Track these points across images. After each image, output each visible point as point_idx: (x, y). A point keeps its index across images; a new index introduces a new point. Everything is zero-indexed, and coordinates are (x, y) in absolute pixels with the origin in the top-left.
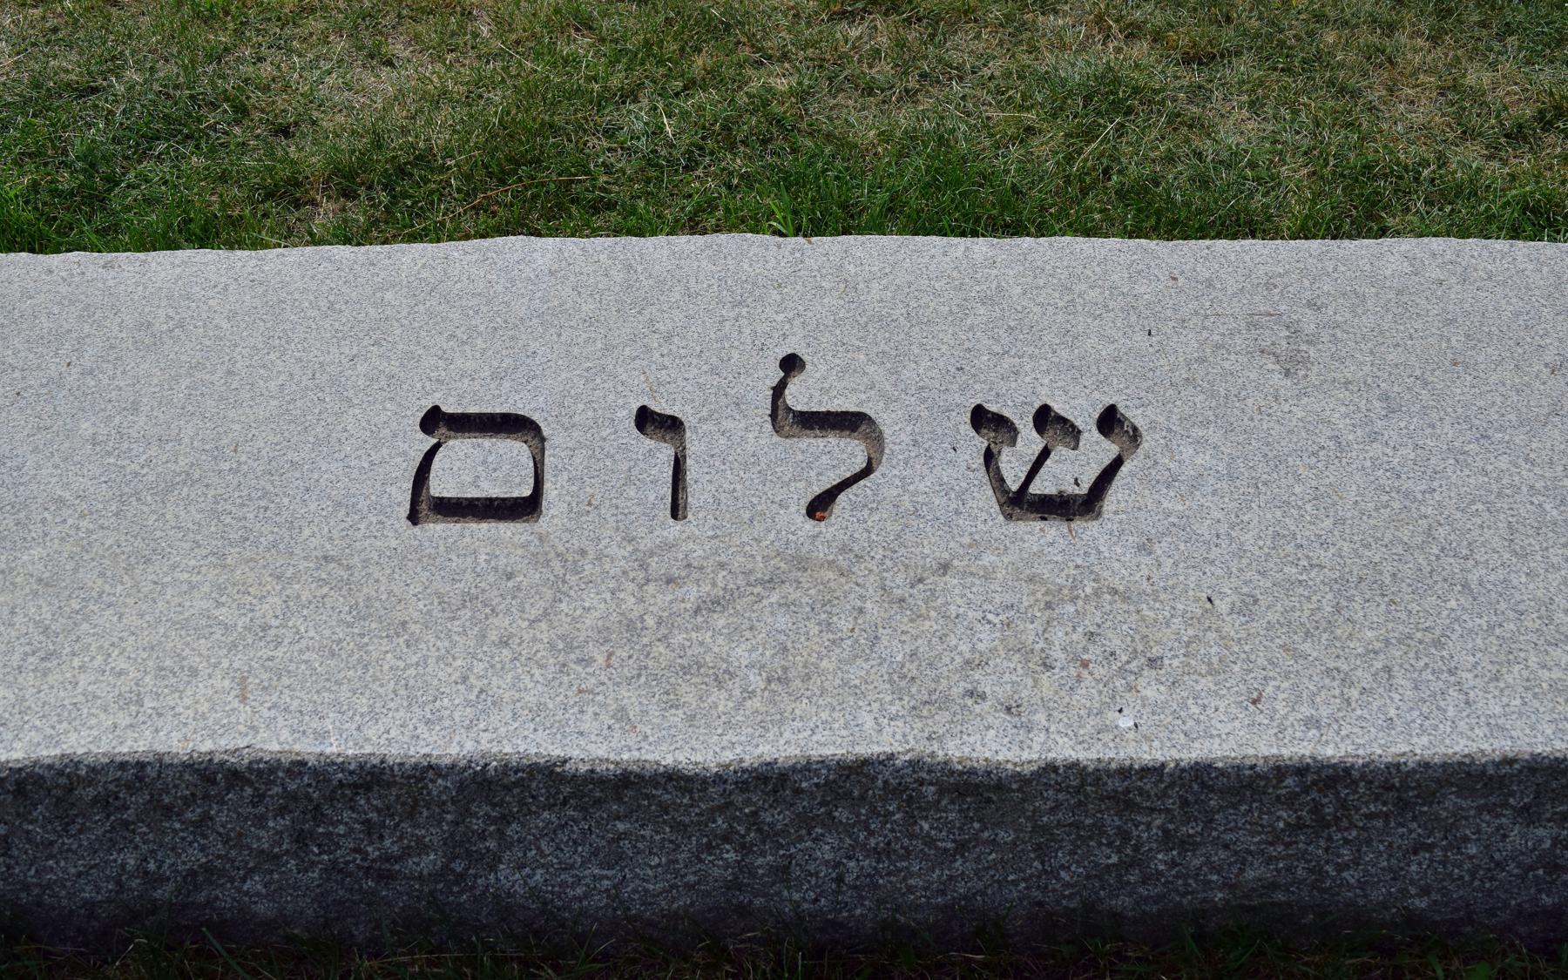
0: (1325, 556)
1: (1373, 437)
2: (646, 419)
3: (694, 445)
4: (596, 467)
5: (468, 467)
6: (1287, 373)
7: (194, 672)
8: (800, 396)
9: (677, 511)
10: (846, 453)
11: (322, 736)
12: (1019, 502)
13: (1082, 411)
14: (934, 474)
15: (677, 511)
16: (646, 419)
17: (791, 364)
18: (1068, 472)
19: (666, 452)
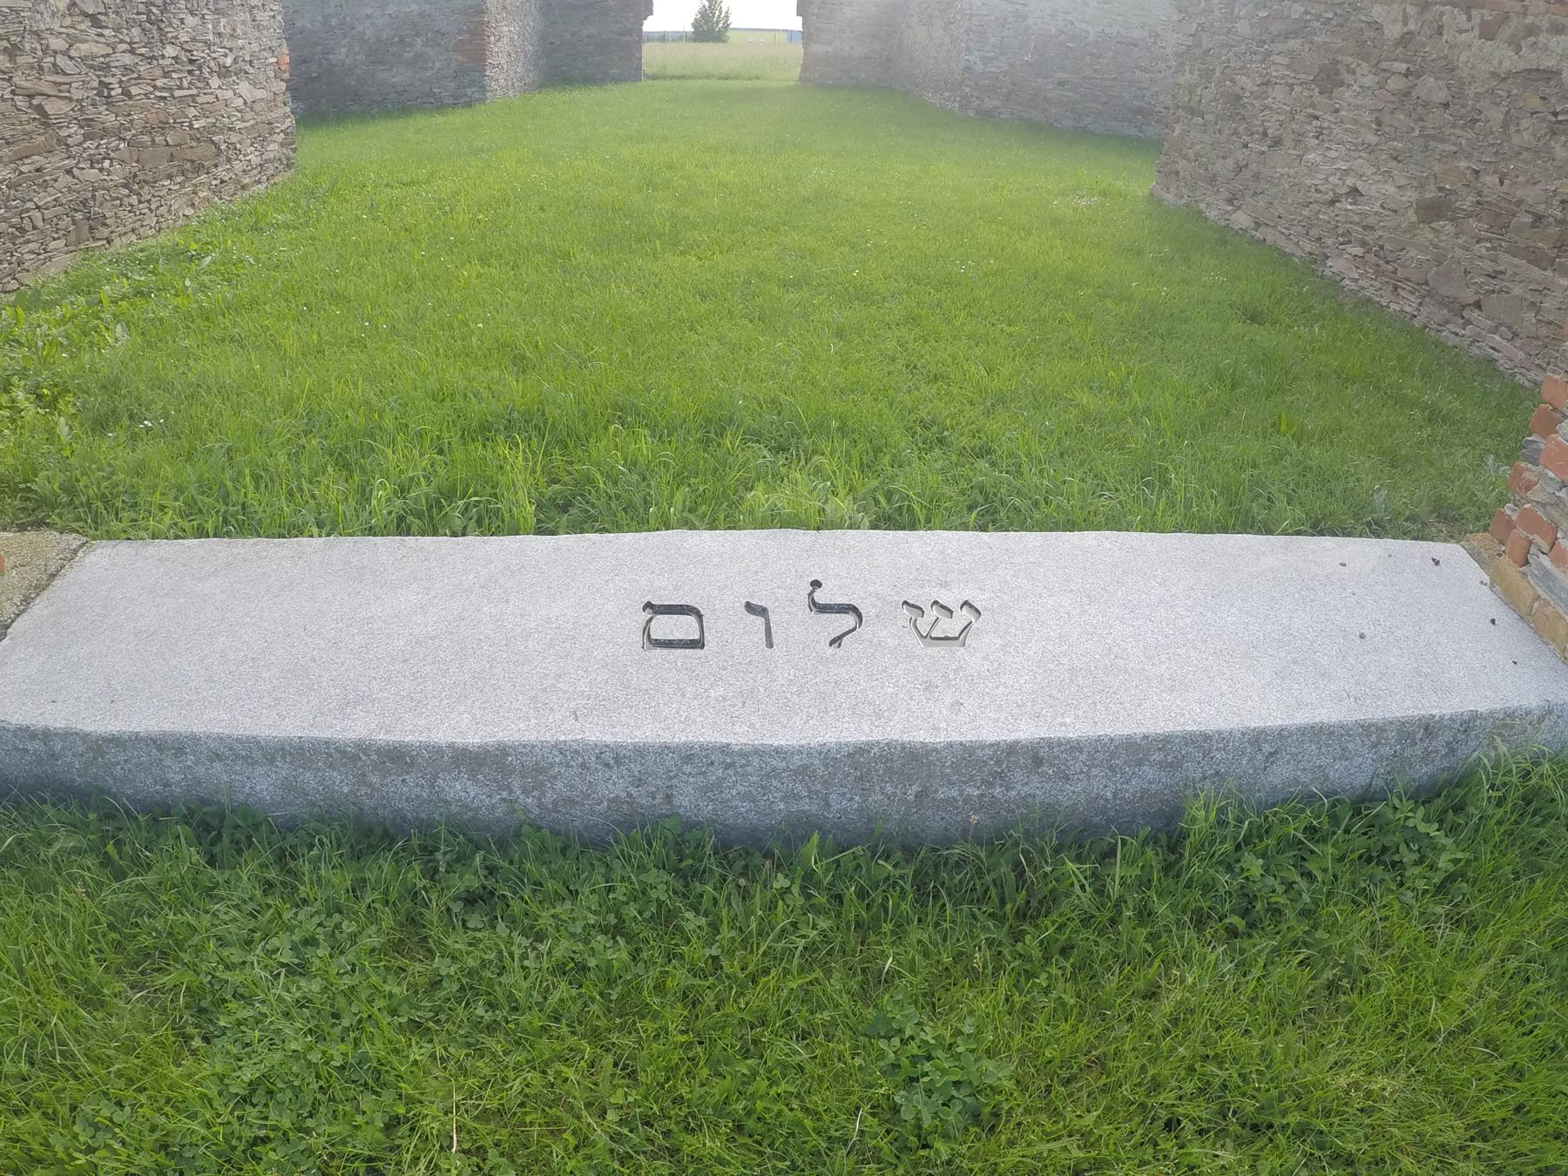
0: (1065, 660)
1: (1084, 612)
2: (750, 607)
3: (773, 618)
4: (730, 631)
5: (683, 627)
6: (342, 953)
7: (552, 709)
8: (821, 597)
9: (770, 645)
10: (849, 620)
11: (615, 735)
12: (930, 638)
13: (951, 599)
14: (792, 619)
15: (770, 645)
16: (750, 607)
17: (816, 584)
18: (949, 627)
19: (760, 621)
